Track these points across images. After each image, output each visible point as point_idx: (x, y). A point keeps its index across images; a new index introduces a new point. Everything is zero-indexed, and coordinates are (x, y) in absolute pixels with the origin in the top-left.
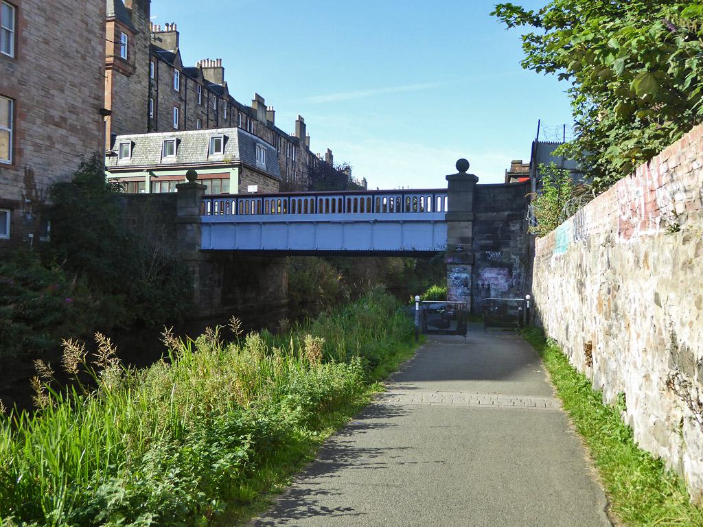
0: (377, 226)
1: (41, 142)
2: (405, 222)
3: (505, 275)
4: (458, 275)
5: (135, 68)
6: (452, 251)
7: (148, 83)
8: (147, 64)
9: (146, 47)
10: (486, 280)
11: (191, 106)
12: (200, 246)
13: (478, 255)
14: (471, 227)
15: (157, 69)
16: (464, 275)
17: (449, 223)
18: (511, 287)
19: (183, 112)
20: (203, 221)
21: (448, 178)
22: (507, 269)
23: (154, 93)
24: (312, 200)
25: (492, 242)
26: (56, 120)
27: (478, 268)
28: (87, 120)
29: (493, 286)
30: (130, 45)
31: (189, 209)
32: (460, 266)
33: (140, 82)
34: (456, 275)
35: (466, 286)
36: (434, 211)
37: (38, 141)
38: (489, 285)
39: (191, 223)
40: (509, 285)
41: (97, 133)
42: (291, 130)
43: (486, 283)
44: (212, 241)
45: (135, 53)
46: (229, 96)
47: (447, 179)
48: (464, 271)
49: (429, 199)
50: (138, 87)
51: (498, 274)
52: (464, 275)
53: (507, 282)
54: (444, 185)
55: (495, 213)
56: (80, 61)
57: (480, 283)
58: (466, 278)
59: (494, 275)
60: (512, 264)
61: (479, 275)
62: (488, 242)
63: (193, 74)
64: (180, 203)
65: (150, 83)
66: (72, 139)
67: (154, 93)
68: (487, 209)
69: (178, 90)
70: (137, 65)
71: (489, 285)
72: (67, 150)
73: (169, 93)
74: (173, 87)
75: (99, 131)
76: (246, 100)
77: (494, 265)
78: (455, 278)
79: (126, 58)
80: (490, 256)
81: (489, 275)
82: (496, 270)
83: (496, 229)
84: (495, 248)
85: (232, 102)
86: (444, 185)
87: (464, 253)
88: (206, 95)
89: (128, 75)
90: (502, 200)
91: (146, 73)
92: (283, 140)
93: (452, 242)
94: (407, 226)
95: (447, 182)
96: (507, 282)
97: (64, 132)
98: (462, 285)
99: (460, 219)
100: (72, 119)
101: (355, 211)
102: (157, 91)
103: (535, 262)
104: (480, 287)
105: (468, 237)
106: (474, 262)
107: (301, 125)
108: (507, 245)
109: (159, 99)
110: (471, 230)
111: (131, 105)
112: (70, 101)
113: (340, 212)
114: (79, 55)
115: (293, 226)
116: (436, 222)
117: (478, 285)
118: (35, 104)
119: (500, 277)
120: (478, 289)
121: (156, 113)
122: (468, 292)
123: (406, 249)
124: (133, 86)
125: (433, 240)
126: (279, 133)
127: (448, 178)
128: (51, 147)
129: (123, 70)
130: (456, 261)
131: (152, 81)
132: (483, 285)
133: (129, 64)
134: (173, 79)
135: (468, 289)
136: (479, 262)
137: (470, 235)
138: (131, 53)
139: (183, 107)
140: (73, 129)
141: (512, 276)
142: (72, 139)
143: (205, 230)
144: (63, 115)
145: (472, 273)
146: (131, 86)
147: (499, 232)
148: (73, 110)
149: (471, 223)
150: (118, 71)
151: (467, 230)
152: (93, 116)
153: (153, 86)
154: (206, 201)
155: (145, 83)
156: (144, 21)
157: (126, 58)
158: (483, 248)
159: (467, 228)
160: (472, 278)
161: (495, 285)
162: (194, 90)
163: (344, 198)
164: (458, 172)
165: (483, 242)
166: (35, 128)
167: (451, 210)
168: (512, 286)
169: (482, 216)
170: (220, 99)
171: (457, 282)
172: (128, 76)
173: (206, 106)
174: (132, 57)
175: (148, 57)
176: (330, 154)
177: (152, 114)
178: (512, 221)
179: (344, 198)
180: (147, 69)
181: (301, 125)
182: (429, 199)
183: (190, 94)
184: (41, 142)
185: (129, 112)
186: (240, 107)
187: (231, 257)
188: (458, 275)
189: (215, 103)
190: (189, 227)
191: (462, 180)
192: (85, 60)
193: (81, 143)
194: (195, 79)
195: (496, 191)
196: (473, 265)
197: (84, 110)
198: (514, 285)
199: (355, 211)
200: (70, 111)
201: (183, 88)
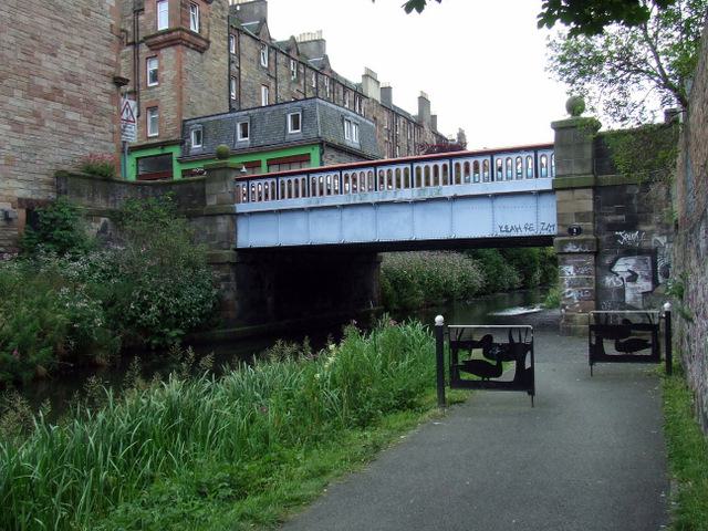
0: (458, 205)
1: (22, 119)
2: (496, 196)
5: (208, 42)
9: (223, 18)
11: (283, 85)
12: (236, 244)
19: (273, 91)
20: (238, 211)
24: (406, 169)
25: (624, 217)
26: (45, 90)
28: (94, 90)
37: (17, 118)
41: (110, 107)
42: (412, 109)
44: (254, 236)
45: (209, 25)
46: (331, 71)
50: (216, 64)
54: (549, 137)
56: (82, 17)
62: (620, 217)
63: (291, 50)
64: (209, 188)
66: (71, 116)
69: (266, 66)
70: (211, 39)
72: (65, 129)
74: (259, 62)
75: (112, 103)
76: (354, 77)
77: (629, 251)
79: (197, 32)
84: (630, 226)
85: (335, 80)
86: (549, 137)
89: (202, 50)
92: (402, 119)
95: (553, 132)
97: (59, 106)
100: (70, 89)
101: (290, 197)
102: (239, 68)
105: (588, 213)
106: (598, 249)
107: (424, 101)
108: (647, 221)
111: (207, 84)
112: (66, 65)
113: (304, 196)
114: (80, 10)
116: (541, 193)
118: (12, 71)
121: (239, 94)
125: (532, 220)
126: (396, 113)
128: (41, 124)
133: (200, 38)
138: (203, 24)
139: (273, 85)
140: (73, 104)
142: (71, 116)
143: (242, 225)
144: (56, 85)
147: (634, 201)
148: (72, 78)
150: (188, 47)
151: (586, 202)
152: (103, 86)
154: (241, 184)
155: (224, 60)
157: (197, 32)
158: (613, 227)
162: (287, 65)
163: (451, 164)
164: (569, 116)
165: (610, 219)
166: (11, 101)
167: (560, 172)
172: (201, 53)
173: (302, 82)
174: (205, 29)
175: (226, 29)
176: (461, 135)
177: (233, 94)
179: (451, 164)
180: (226, 43)
181: (424, 101)
183: (282, 71)
184: (22, 119)
185: (204, 93)
186: (346, 87)
189: (313, 79)
190: (220, 220)
192: (89, 15)
193: (86, 120)
197: (88, 78)
199: (297, 196)
200: (67, 80)
201: (272, 64)
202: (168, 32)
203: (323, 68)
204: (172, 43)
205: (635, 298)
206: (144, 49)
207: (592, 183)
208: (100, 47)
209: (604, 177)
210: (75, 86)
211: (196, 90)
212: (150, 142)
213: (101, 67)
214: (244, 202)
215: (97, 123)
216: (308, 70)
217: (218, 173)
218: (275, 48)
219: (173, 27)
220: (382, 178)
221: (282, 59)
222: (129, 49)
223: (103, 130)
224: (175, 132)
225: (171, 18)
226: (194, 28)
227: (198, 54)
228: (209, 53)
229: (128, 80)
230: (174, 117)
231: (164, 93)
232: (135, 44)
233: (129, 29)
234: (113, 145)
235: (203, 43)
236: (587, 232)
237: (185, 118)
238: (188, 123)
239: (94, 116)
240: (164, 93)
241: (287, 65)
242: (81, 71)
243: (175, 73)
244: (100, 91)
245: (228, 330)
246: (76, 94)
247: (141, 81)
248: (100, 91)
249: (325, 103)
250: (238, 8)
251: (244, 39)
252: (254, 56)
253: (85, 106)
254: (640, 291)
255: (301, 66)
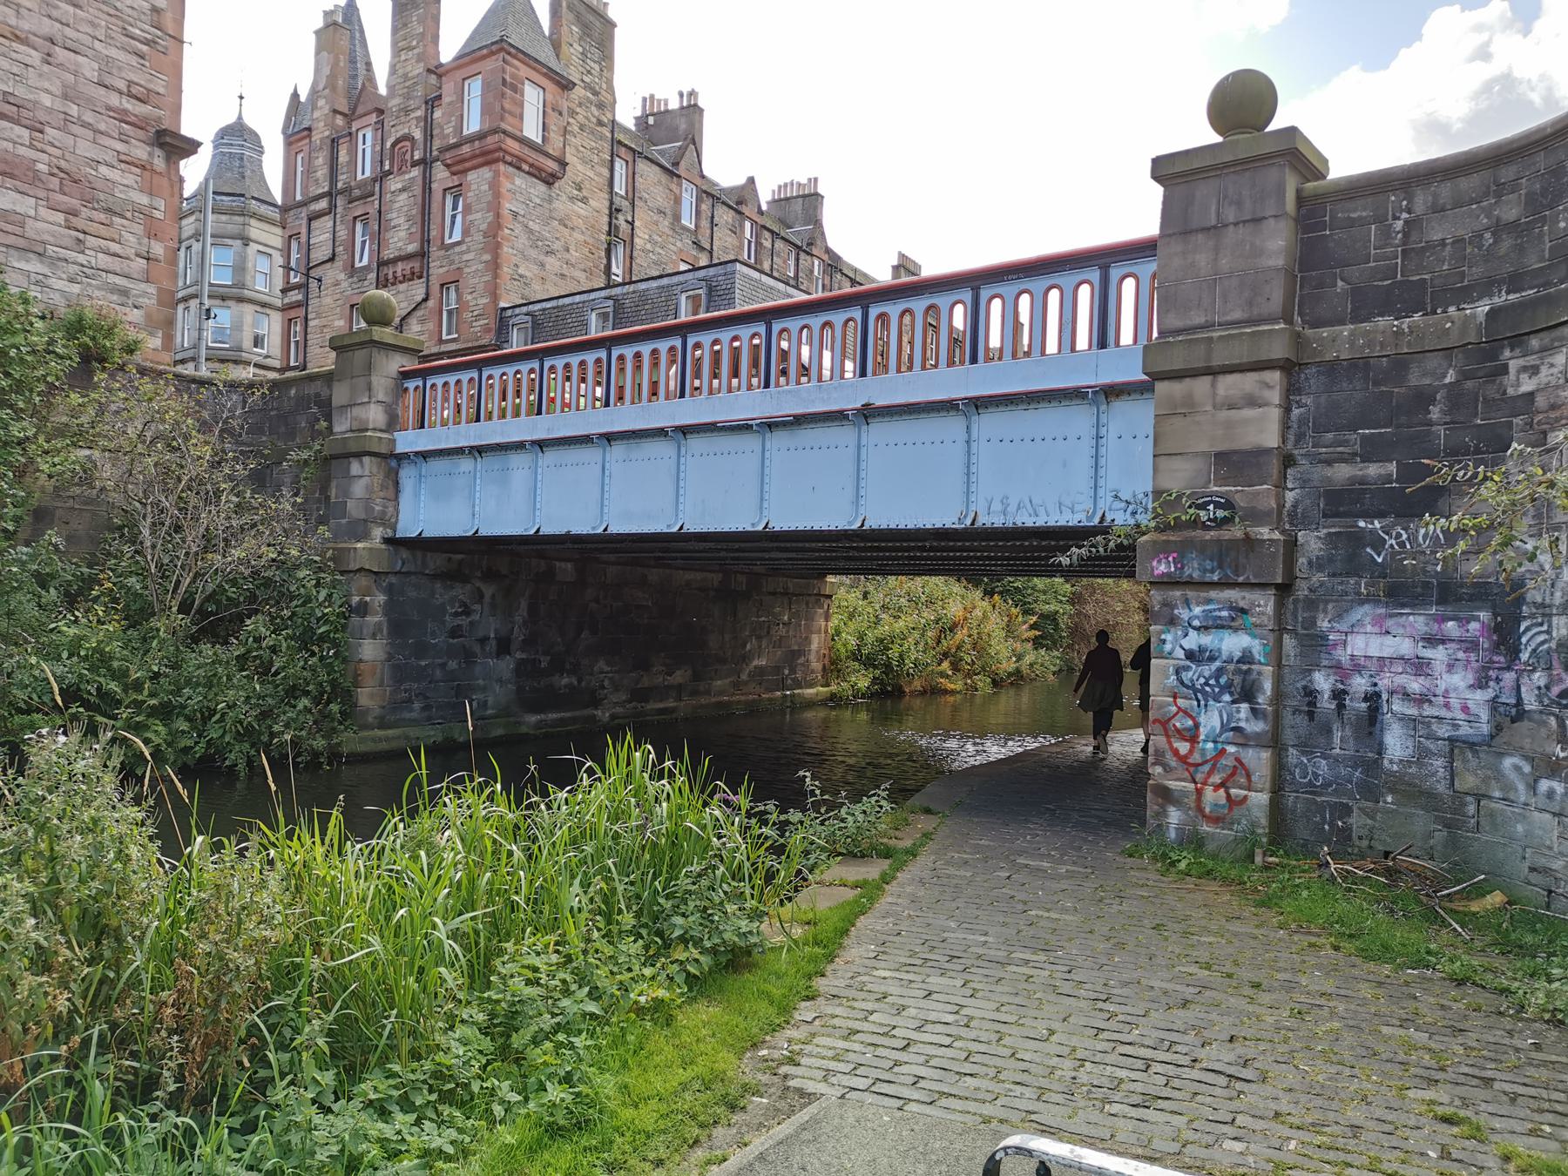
0: (879, 431)
3: (1471, 645)
4: (1207, 640)
5: (563, 164)
6: (1174, 520)
7: (607, 204)
8: (603, 160)
9: (600, 123)
10: (1358, 668)
13: (1312, 542)
14: (1275, 396)
15: (633, 175)
16: (1232, 643)
17: (1161, 387)
18: (1510, 715)
20: (400, 449)
21: (1166, 170)
22: (1484, 615)
23: (623, 226)
25: (1392, 468)
27: (1312, 604)
29: (1398, 706)
30: (549, 110)
31: (356, 411)
32: (1213, 594)
33: (584, 200)
34: (1193, 641)
35: (1247, 694)
36: (1103, 345)
38: (1373, 698)
39: (359, 455)
40: (1494, 703)
43: (1360, 684)
44: (434, 510)
46: (828, 251)
47: (1156, 176)
48: (1237, 618)
49: (1084, 292)
51: (1431, 641)
52: (1232, 643)
53: (1481, 684)
54: (1140, 212)
55: (1417, 317)
57: (1323, 682)
58: (1247, 658)
59: (1406, 647)
60: (1518, 584)
61: (1316, 646)
62: (1373, 470)
65: (612, 203)
67: (623, 226)
68: (1364, 305)
71: (1373, 698)
73: (667, 230)
74: (677, 217)
77: (1401, 591)
78: (1190, 655)
79: (539, 141)
80: (1378, 544)
81: (1373, 641)
82: (1418, 622)
83: (1424, 398)
87: (1236, 532)
88: (768, 244)
89: (550, 180)
90: (1459, 241)
91: (603, 181)
93: (1180, 476)
94: (990, 423)
96: (1481, 684)
98: (1228, 688)
99: (1216, 362)
102: (632, 224)
103: (917, 584)
104: (1326, 704)
109: (637, 240)
110: (1275, 414)
115: (618, 450)
116: (1112, 392)
117: (1311, 694)
119: (1439, 655)
120: (1311, 715)
122: (1256, 727)
123: (985, 520)
124: (562, 206)
127: (1166, 170)
129: (531, 165)
130: (1193, 570)
131: (617, 200)
132: (1339, 695)
133: (547, 155)
134: (678, 200)
135: (1255, 712)
136: (1319, 577)
137: (1271, 439)
141: (1514, 652)
145: (1280, 630)
146: (556, 204)
147: (1435, 413)
149: (1275, 377)
150: (519, 168)
152: (120, 146)
153: (618, 211)
155: (600, 203)
156: (597, 67)
157: (539, 141)
159: (1252, 402)
160: (1277, 657)
161: (1406, 696)
162: (736, 231)
168: (1520, 714)
169: (1340, 340)
170: (802, 255)
171: (1197, 674)
172: (549, 184)
175: (607, 146)
178: (1517, 341)
180: (606, 172)
182: (1084, 292)
187: (566, 570)
188: (1207, 640)
190: (355, 468)
191: (1242, 155)
194: (739, 208)
195: (1421, 201)
196: (1284, 590)
198: (1530, 702)
201: (705, 224)
202: (481, 136)
203: (809, 244)
204: (489, 158)
205: (1422, 754)
206: (440, 174)
207: (1278, 350)
208: (113, 52)
209: (1325, 332)
210: (26, 133)
211: (533, 253)
212: (444, 348)
213: (115, 100)
214: (444, 423)
215: (93, 228)
216: (779, 244)
217: (360, 355)
218: (710, 195)
219: (487, 126)
220: (698, 362)
221: (725, 216)
222: (416, 172)
223: (115, 247)
224: (487, 330)
225: (486, 110)
226: (532, 131)
227: (542, 187)
228: (564, 186)
229: (199, 144)
230: (485, 301)
231: (470, 256)
232: (426, 163)
233: (418, 134)
234: (152, 289)
235: (552, 166)
236: (1255, 516)
237: (503, 304)
238: (509, 313)
239: (85, 212)
240: (470, 256)
241: (736, 231)
242: (47, 101)
243: (490, 216)
244: (109, 157)
245: (661, 705)
246: (22, 151)
247: (433, 233)
248: (109, 157)
249: (756, 275)
250: (651, 120)
251: (642, 166)
252: (667, 205)
253: (54, 183)
254: (1443, 731)
255: (767, 234)
